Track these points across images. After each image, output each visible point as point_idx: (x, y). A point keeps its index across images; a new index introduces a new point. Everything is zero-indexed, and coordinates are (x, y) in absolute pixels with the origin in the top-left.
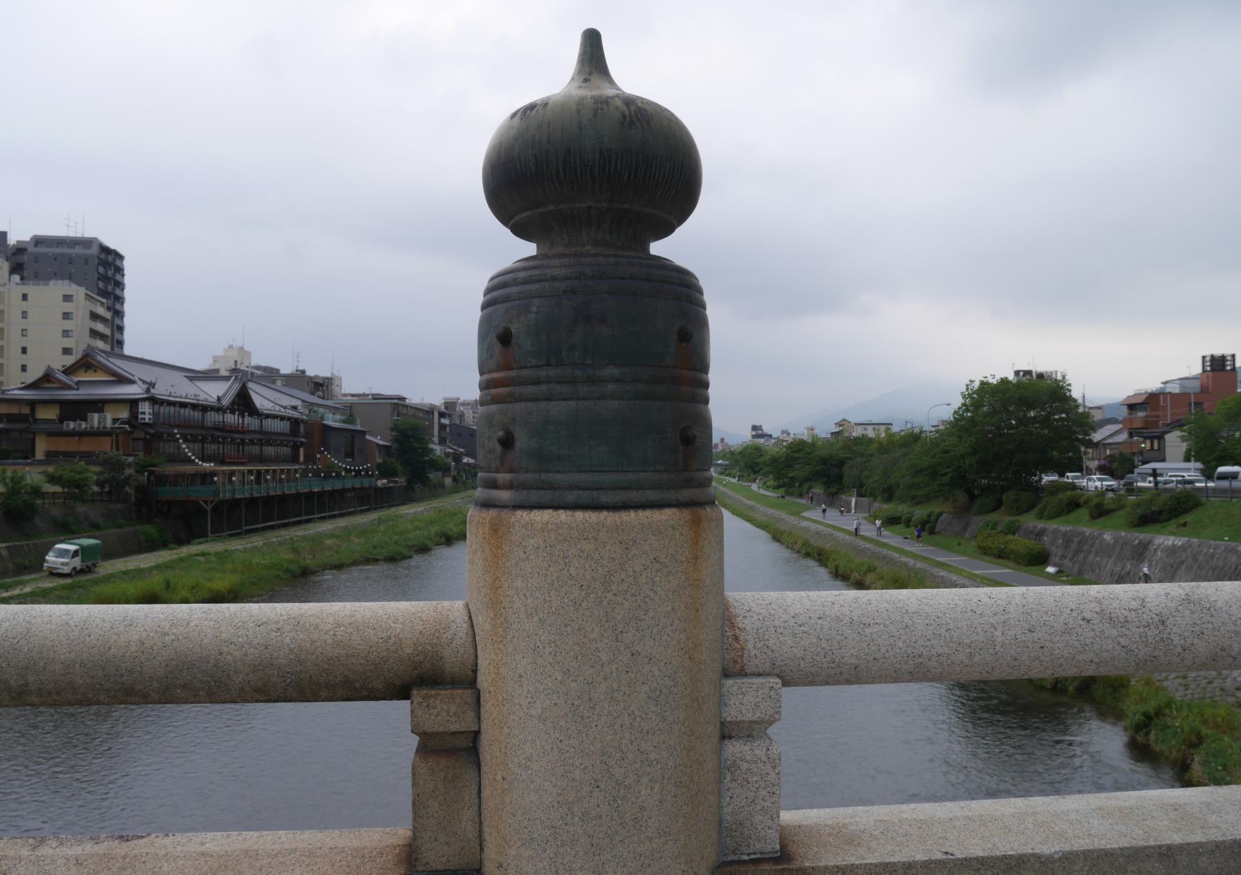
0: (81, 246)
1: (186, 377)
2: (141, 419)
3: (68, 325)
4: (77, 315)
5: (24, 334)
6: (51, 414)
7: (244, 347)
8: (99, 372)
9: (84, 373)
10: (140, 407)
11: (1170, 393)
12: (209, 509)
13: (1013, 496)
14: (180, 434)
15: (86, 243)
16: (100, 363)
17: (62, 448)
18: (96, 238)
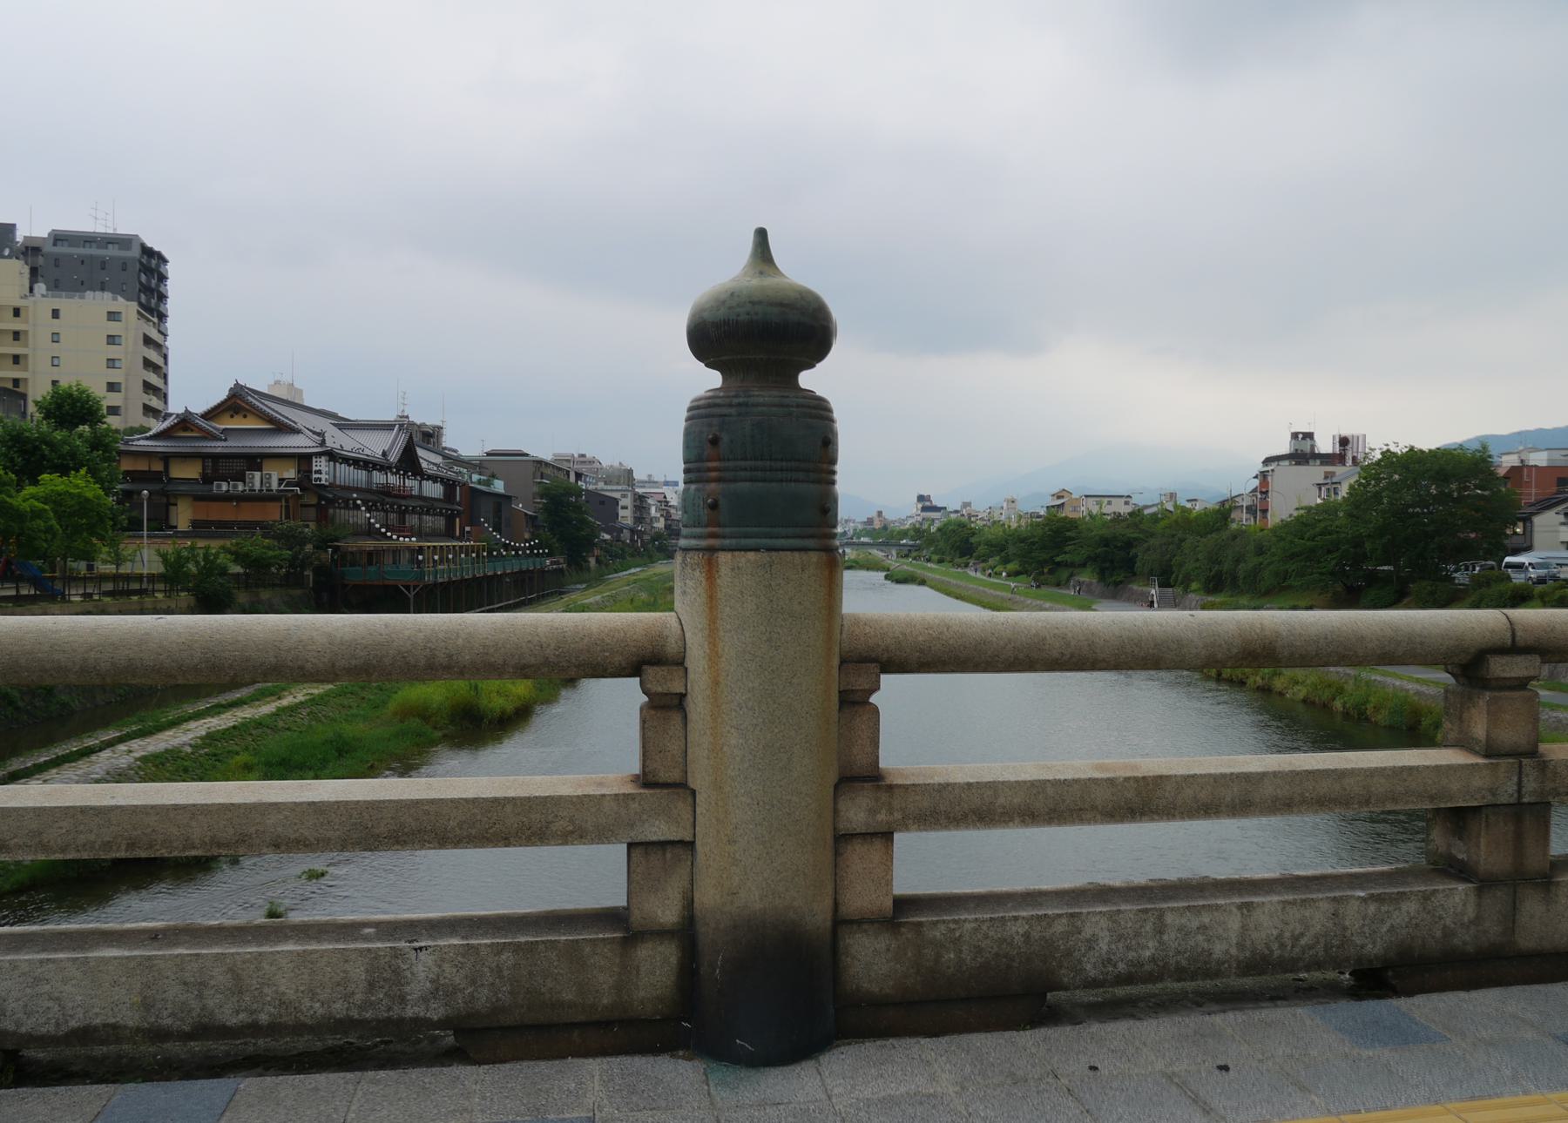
0: (116, 246)
1: (333, 424)
2: (316, 479)
3: (114, 353)
4: (126, 339)
5: (56, 362)
6: (191, 471)
7: (295, 383)
8: (250, 417)
9: (231, 419)
10: (314, 464)
11: (1536, 466)
12: (411, 596)
13: (1429, 588)
14: (361, 500)
15: (125, 242)
16: (253, 406)
17: (214, 517)
18: (137, 236)
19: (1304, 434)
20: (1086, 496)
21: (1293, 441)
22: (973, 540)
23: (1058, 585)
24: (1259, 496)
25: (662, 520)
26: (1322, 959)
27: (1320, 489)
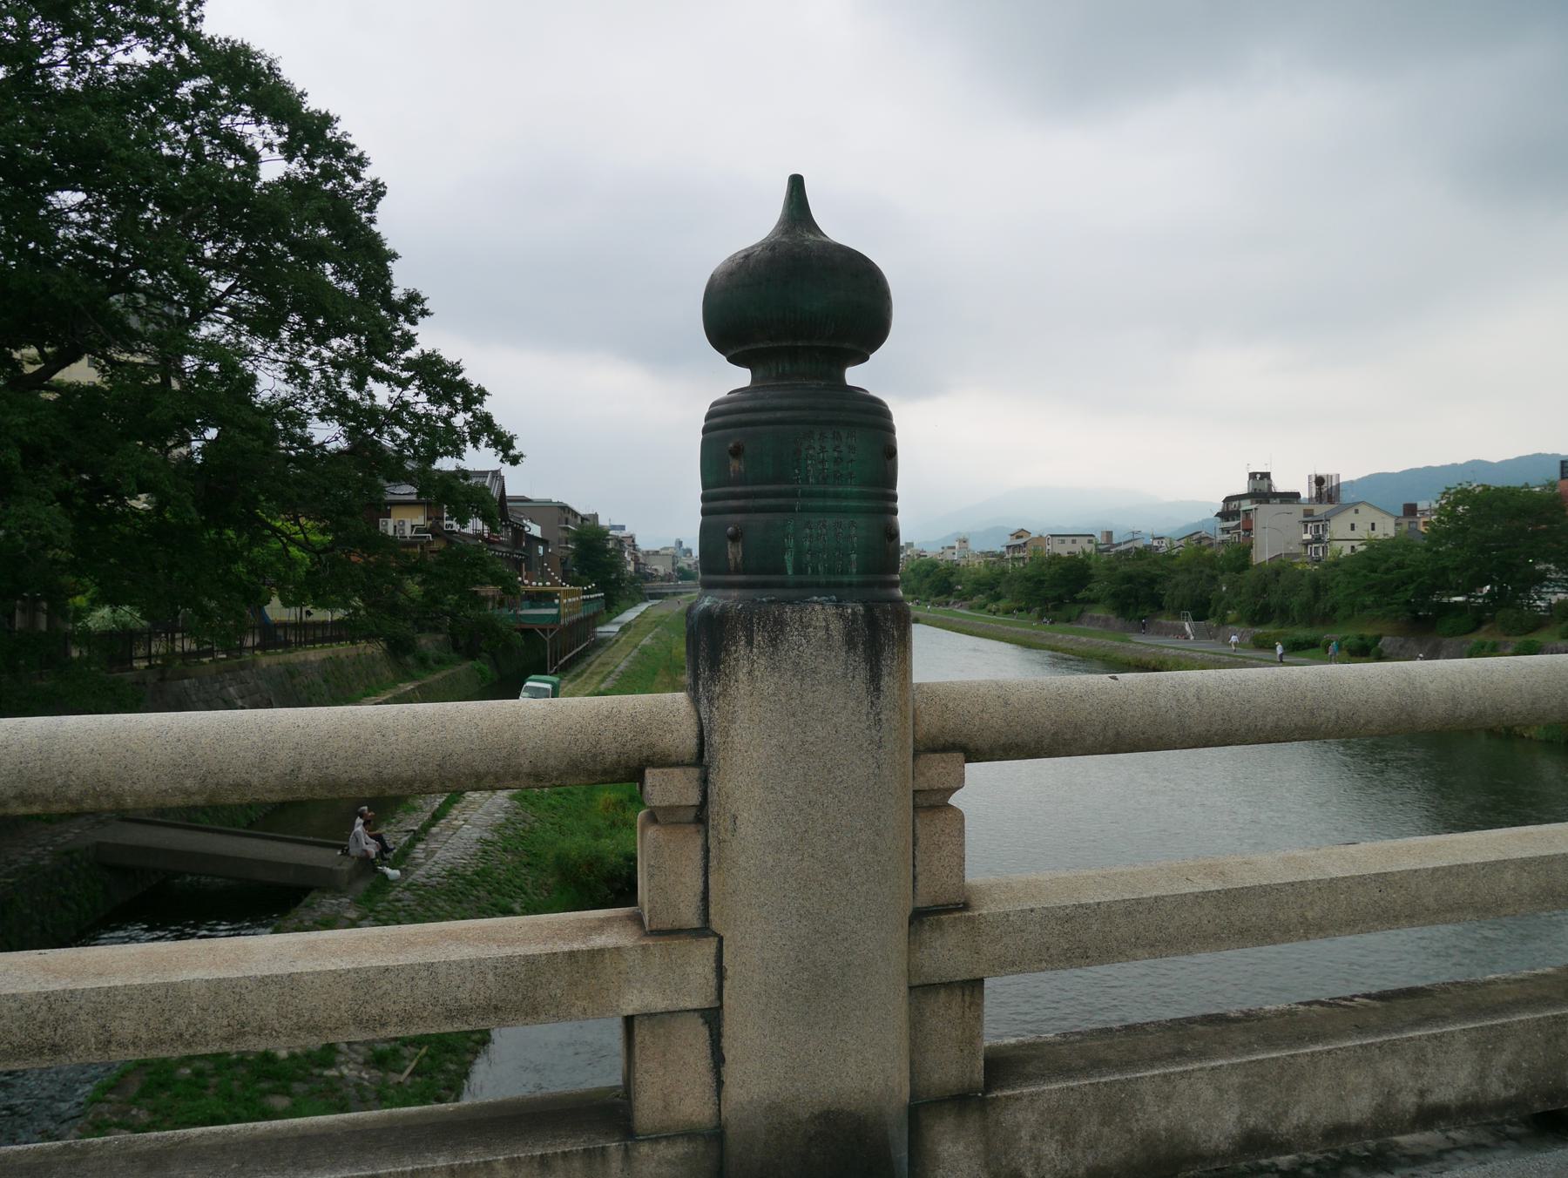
2: (447, 526)
19: (1262, 474)
20: (1052, 536)
22: (952, 579)
23: (1069, 621)
24: (1243, 533)
25: (632, 563)
27: (1306, 526)
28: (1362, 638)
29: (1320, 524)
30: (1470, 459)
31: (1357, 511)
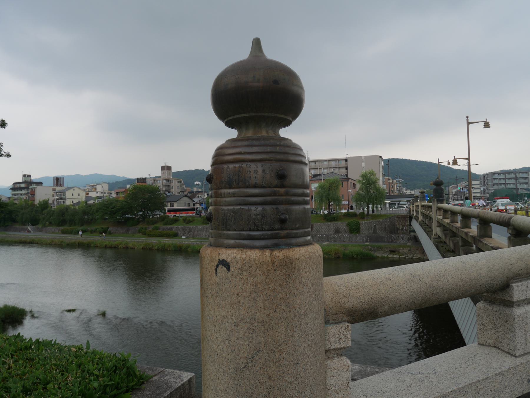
21: (24, 177)
24: (30, 196)
26: (5, 325)
28: (102, 228)
29: (62, 193)
30: (179, 171)
31: (74, 190)
